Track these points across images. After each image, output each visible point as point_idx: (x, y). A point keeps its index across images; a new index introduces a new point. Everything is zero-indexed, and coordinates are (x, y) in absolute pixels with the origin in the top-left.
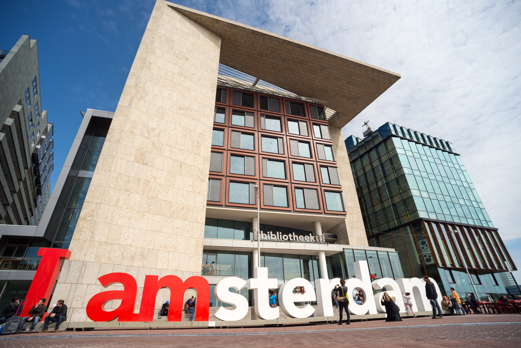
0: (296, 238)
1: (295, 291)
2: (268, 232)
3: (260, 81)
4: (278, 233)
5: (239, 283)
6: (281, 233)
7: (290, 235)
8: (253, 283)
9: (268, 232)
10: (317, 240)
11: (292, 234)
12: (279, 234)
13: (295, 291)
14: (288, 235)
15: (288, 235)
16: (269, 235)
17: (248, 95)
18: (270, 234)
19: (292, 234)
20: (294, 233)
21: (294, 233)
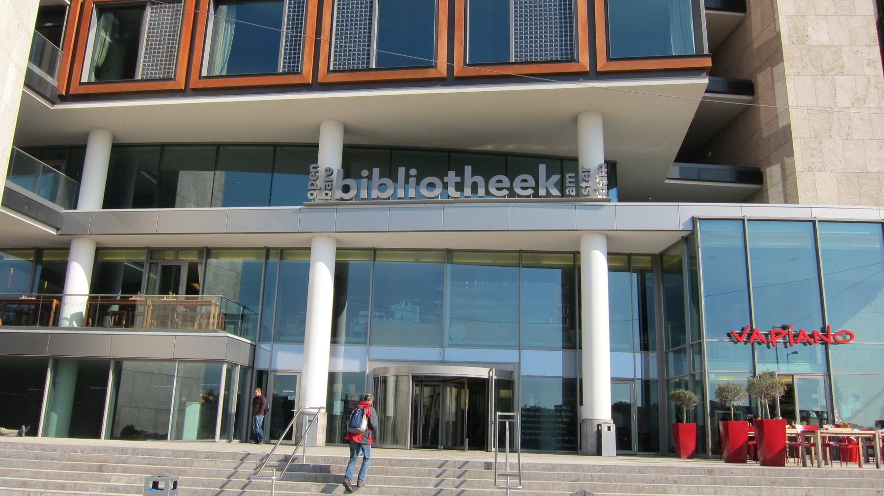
4: (402, 171)
6: (413, 172)
9: (365, 173)
11: (460, 173)
19: (460, 173)
20: (468, 169)
21: (468, 169)
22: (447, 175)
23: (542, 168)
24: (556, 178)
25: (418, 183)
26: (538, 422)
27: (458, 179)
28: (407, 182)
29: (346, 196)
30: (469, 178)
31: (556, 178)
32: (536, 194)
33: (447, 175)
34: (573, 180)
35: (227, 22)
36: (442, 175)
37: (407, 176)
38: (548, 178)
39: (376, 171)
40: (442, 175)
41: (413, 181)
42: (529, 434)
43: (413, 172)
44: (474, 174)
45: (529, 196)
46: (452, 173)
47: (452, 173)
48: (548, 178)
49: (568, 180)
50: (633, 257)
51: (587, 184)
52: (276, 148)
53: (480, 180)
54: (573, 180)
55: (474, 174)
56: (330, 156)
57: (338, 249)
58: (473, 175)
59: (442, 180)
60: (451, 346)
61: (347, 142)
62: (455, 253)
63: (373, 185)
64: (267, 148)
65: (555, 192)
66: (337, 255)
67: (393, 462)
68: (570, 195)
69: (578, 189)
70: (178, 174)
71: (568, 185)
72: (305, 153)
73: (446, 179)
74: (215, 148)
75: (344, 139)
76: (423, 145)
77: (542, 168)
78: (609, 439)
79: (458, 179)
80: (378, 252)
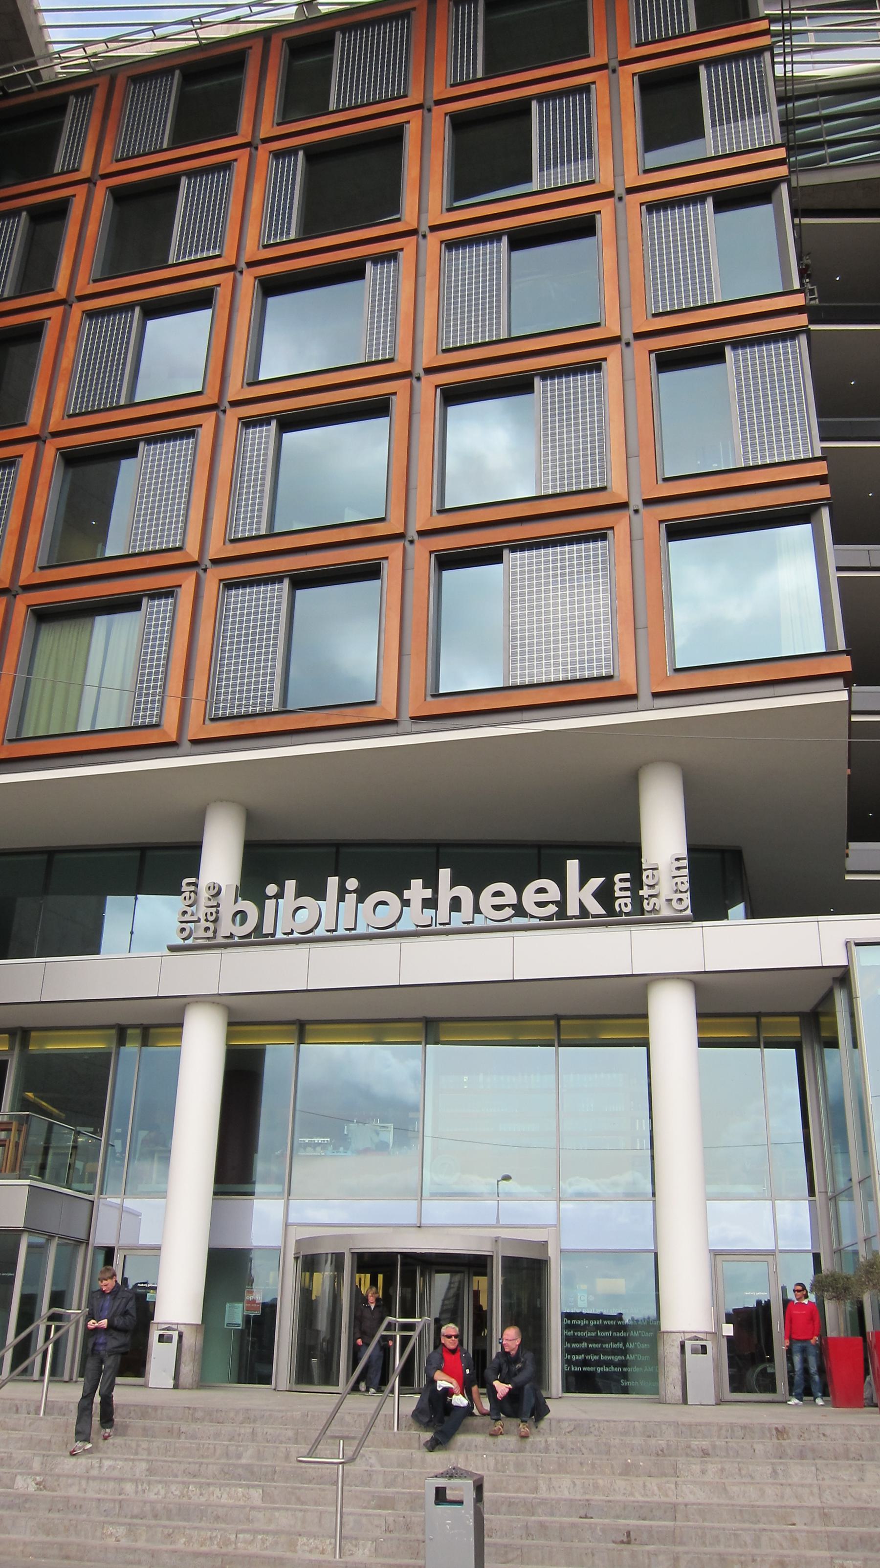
4: (333, 882)
6: (352, 883)
10: (623, 902)
11: (432, 883)
19: (432, 883)
20: (445, 874)
21: (445, 874)
23: (573, 867)
24: (595, 883)
25: (361, 900)
26: (624, 1340)
27: (428, 893)
28: (341, 899)
29: (212, 929)
30: (446, 892)
31: (595, 883)
32: (562, 913)
34: (628, 885)
35: (90, 943)
36: (399, 887)
37: (343, 892)
38: (583, 883)
39: (291, 885)
40: (399, 887)
41: (351, 898)
42: (577, 1363)
43: (352, 883)
44: (455, 882)
45: (550, 918)
47: (417, 883)
48: (583, 883)
49: (618, 885)
50: (764, 1020)
51: (652, 892)
52: (539, 846)
53: (464, 893)
54: (628, 885)
55: (455, 882)
56: (221, 860)
57: (230, 1024)
59: (400, 896)
60: (435, 1195)
62: (443, 1025)
63: (289, 908)
64: (37, 857)
65: (594, 907)
66: (230, 1036)
67: (199, 1414)
68: (621, 913)
69: (638, 902)
71: (618, 894)
72: (268, 862)
73: (407, 894)
74: (137, 854)
77: (573, 867)
78: (707, 1372)
79: (428, 893)
80: (308, 1027)
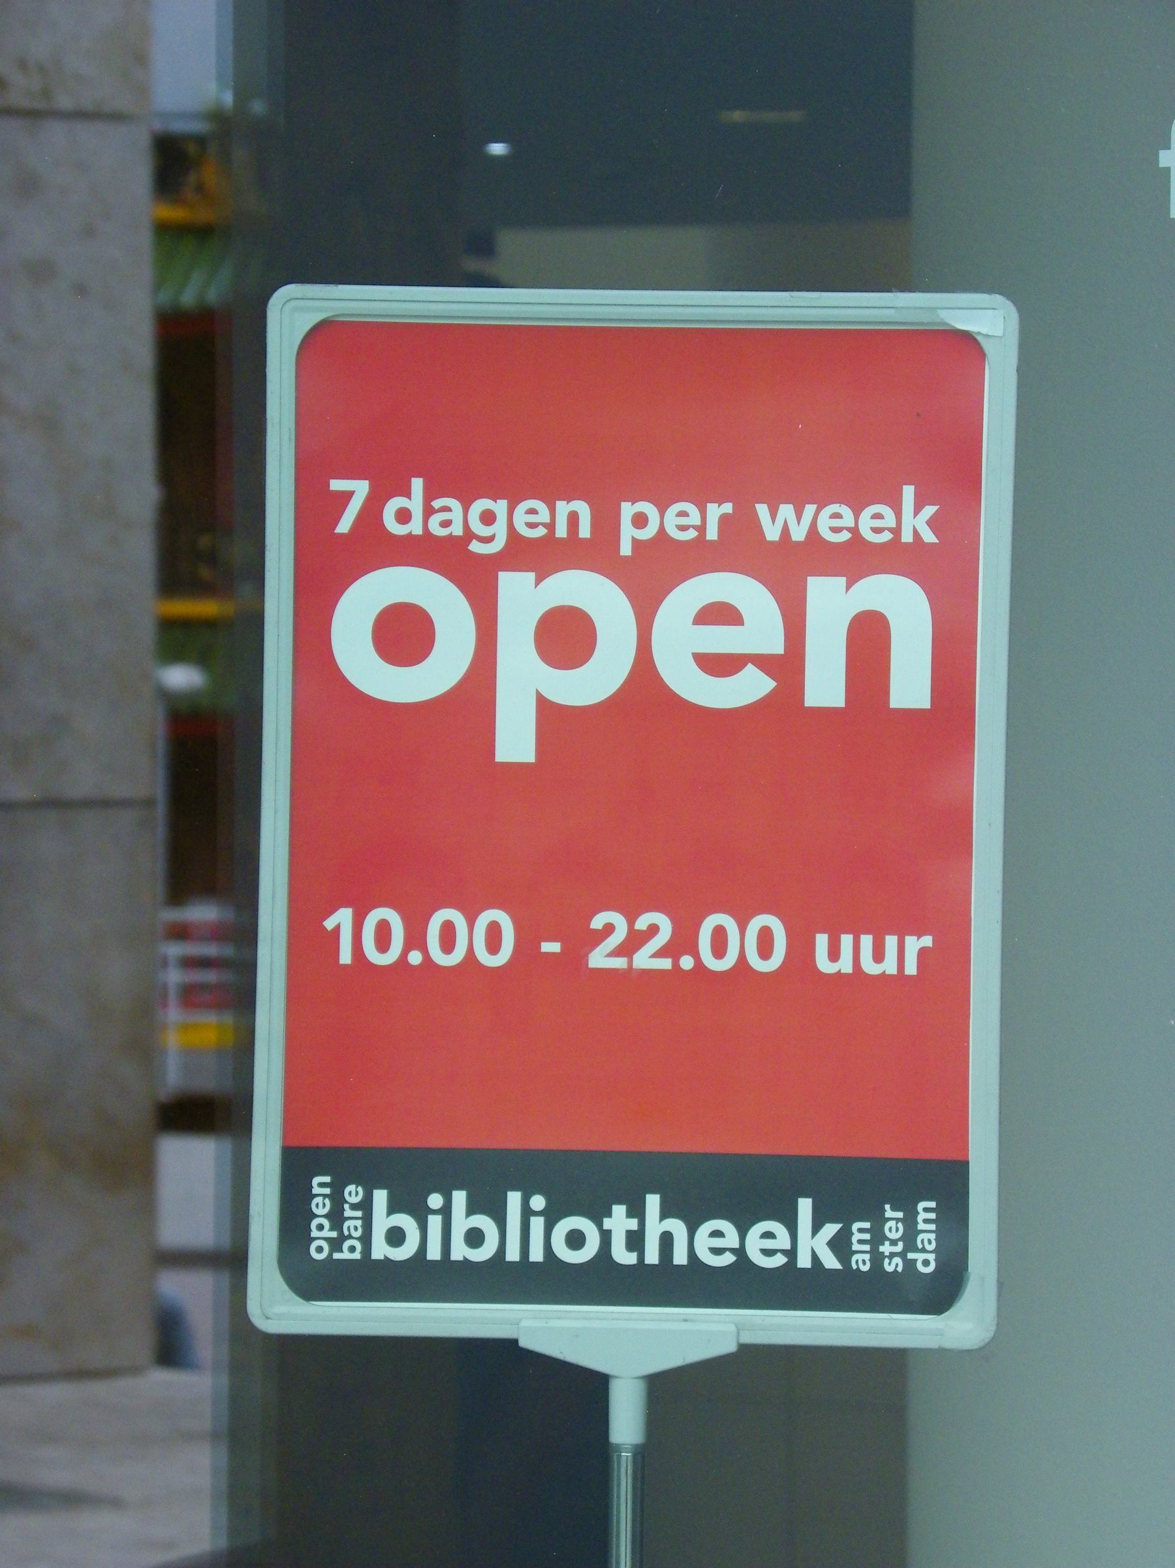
0: (667, 1240)
1: (831, 517)
2: (435, 1201)
3: (625, 966)
4: (514, 1199)
5: (887, 1261)
6: (538, 1202)
7: (619, 1221)
8: (887, 1254)
9: (435, 1201)
11: (637, 1210)
12: (527, 1213)
13: (831, 517)
14: (598, 1214)
15: (598, 1214)
16: (435, 1223)
17: (673, 1320)
18: (446, 1211)
19: (637, 1210)
20: (653, 1202)
21: (653, 1202)
22: (610, 1215)
24: (831, 1229)
27: (633, 1224)
31: (831, 1229)
33: (610, 1215)
34: (867, 1236)
43: (538, 1202)
46: (619, 1210)
47: (619, 1210)
54: (867, 1236)
58: (391, 1211)
59: (599, 1225)
61: (296, 1142)
70: (593, 969)
73: (607, 1223)
75: (285, 1137)
76: (228, 1169)
79: (633, 1224)
